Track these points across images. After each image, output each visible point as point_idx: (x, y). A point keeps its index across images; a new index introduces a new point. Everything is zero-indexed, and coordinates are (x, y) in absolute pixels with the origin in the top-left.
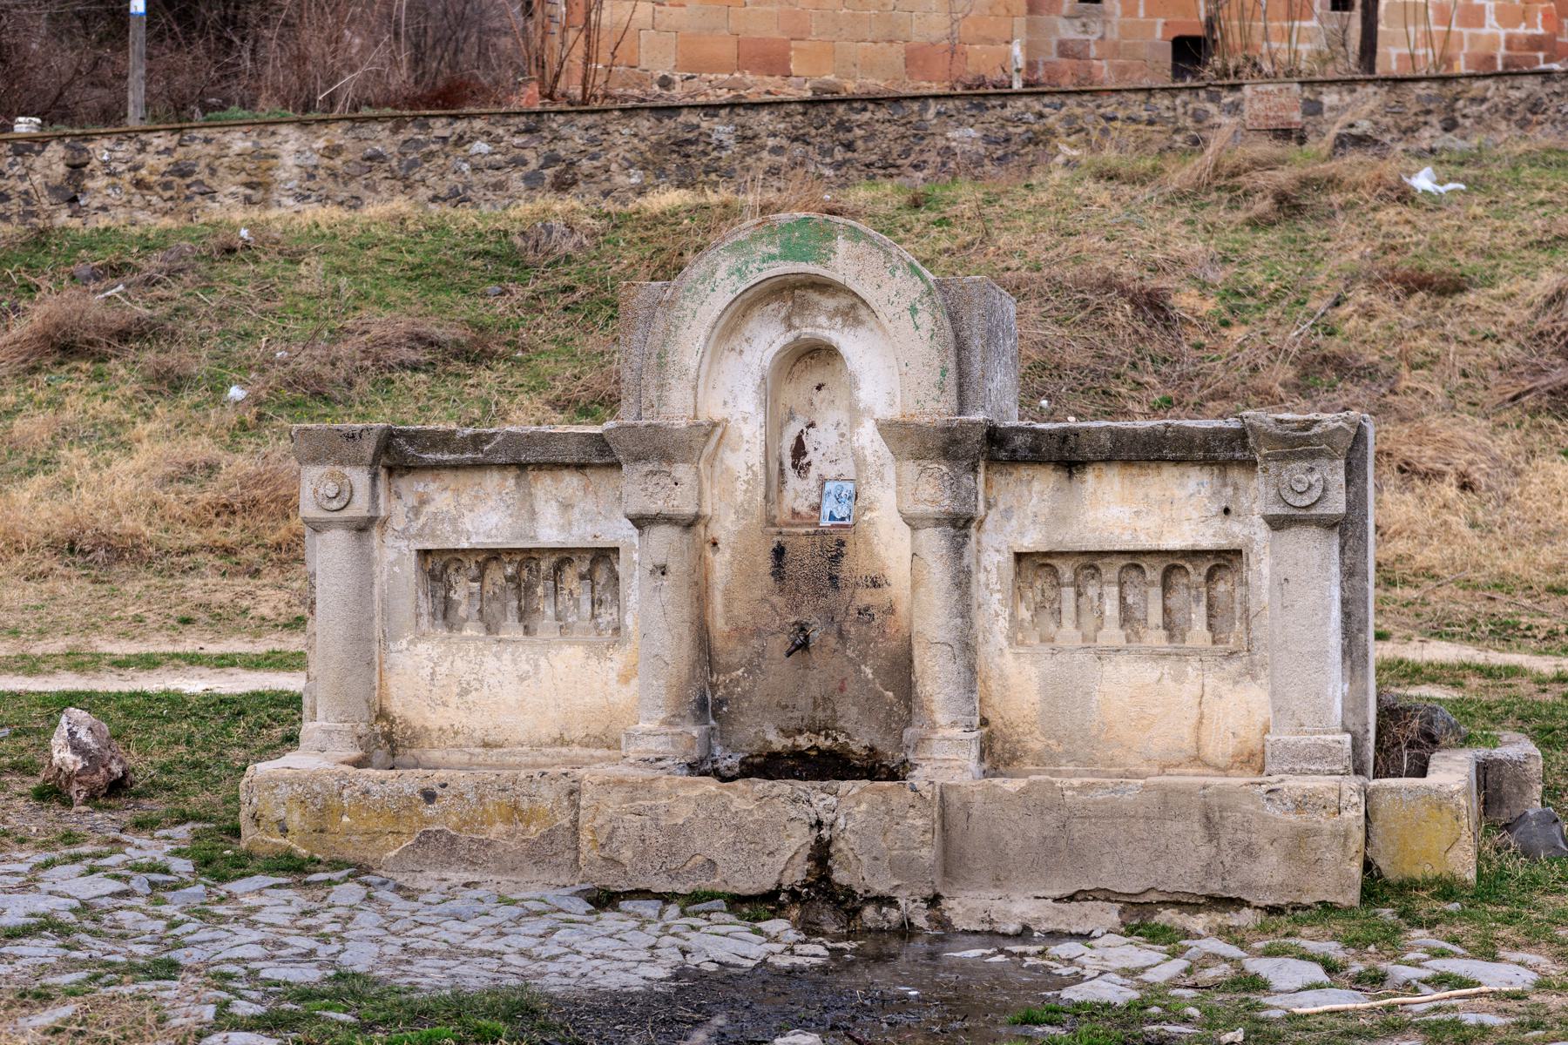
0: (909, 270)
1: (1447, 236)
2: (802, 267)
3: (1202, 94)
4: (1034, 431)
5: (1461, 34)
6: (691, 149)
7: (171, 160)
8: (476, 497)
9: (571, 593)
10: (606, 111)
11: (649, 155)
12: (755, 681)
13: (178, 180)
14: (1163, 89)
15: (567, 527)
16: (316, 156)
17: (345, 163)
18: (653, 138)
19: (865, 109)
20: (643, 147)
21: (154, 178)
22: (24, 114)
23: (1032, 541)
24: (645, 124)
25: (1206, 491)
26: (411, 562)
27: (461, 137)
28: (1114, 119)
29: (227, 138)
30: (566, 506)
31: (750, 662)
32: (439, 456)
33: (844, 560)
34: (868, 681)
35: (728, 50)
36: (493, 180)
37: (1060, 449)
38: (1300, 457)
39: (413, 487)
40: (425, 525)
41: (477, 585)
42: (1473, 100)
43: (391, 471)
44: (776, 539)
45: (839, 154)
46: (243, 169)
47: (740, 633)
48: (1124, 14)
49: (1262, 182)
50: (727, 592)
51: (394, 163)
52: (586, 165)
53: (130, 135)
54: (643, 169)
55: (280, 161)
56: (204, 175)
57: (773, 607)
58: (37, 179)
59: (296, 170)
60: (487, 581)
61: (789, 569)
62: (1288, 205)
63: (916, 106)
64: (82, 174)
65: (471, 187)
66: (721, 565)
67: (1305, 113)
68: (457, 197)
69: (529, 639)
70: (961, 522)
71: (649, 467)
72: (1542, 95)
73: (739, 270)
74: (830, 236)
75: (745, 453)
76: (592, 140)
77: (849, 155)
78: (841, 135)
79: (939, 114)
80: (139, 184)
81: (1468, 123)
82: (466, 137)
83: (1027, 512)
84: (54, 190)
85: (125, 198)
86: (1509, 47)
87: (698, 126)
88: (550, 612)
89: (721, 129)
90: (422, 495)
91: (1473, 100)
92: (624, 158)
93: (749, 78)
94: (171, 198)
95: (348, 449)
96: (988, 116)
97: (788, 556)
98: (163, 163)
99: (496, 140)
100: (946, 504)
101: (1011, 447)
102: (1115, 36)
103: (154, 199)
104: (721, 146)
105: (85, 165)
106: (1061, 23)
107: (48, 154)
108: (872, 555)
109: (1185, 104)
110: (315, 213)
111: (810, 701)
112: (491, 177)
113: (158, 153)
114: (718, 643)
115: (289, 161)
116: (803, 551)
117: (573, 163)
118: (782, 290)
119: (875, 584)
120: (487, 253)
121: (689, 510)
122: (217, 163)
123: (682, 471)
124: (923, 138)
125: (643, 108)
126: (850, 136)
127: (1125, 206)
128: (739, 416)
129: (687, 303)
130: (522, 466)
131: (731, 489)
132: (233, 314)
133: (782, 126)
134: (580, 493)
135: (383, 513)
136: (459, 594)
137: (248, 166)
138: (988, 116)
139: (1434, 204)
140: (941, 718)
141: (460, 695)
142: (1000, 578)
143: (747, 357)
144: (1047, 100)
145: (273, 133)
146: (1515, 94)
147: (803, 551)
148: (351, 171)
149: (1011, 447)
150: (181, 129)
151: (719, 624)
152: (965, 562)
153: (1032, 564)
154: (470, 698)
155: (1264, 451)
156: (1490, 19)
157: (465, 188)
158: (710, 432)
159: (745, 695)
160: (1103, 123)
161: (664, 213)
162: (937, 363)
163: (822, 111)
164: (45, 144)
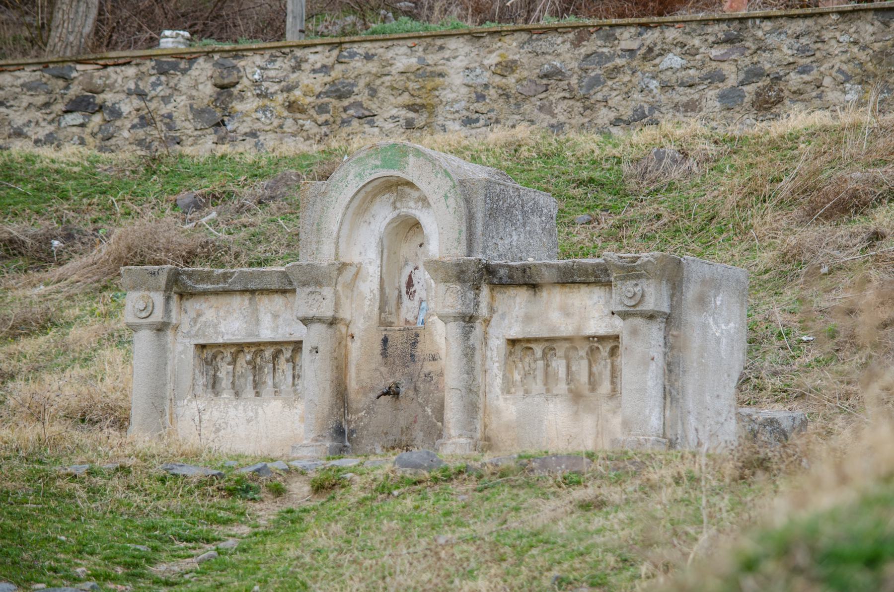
0: (444, 174)
2: (391, 172)
4: (508, 266)
7: (327, 79)
8: (228, 312)
9: (283, 372)
11: (870, 66)
12: (370, 418)
13: (335, 102)
15: (275, 328)
16: (487, 74)
17: (518, 81)
18: (877, 46)
20: (863, 56)
21: (308, 100)
22: (171, 28)
23: (515, 332)
25: (602, 301)
26: (191, 351)
27: (650, 50)
29: (390, 54)
30: (276, 316)
31: (369, 407)
32: (205, 286)
33: (418, 345)
34: (428, 417)
36: (685, 99)
37: (524, 277)
38: (632, 278)
39: (193, 305)
40: (199, 329)
41: (231, 367)
43: (181, 296)
44: (384, 333)
46: (406, 89)
47: (365, 391)
50: (358, 366)
51: (574, 81)
52: (794, 80)
53: (285, 51)
55: (447, 80)
56: (363, 97)
57: (381, 373)
58: (181, 100)
59: (464, 90)
60: (238, 364)
61: (390, 351)
64: (230, 95)
65: (658, 108)
66: (355, 349)
68: (640, 118)
69: (259, 398)
70: (467, 319)
71: (310, 289)
73: (360, 174)
75: (369, 286)
80: (291, 106)
82: (656, 50)
83: (513, 314)
84: (199, 113)
85: (276, 123)
88: (270, 382)
90: (199, 310)
92: (840, 71)
94: (326, 123)
95: (152, 281)
97: (390, 343)
98: (317, 83)
100: (459, 308)
101: (498, 276)
103: (308, 124)
105: (234, 85)
107: (194, 73)
108: (433, 342)
111: (400, 429)
112: (682, 95)
113: (314, 71)
114: (352, 396)
115: (456, 79)
116: (398, 340)
118: (392, 186)
119: (434, 359)
120: (591, 180)
121: (327, 312)
122: (378, 82)
123: (327, 291)
128: (367, 261)
129: (333, 194)
130: (253, 292)
131: (361, 311)
134: (283, 309)
135: (174, 321)
136: (221, 374)
137: (411, 85)
141: (215, 433)
142: (498, 354)
143: (372, 227)
145: (441, 48)
147: (398, 340)
148: (524, 91)
149: (498, 276)
150: (341, 43)
151: (353, 385)
152: (471, 342)
153: (516, 344)
154: (220, 434)
155: (615, 275)
157: (652, 109)
159: (365, 427)
162: (457, 227)
164: (192, 61)
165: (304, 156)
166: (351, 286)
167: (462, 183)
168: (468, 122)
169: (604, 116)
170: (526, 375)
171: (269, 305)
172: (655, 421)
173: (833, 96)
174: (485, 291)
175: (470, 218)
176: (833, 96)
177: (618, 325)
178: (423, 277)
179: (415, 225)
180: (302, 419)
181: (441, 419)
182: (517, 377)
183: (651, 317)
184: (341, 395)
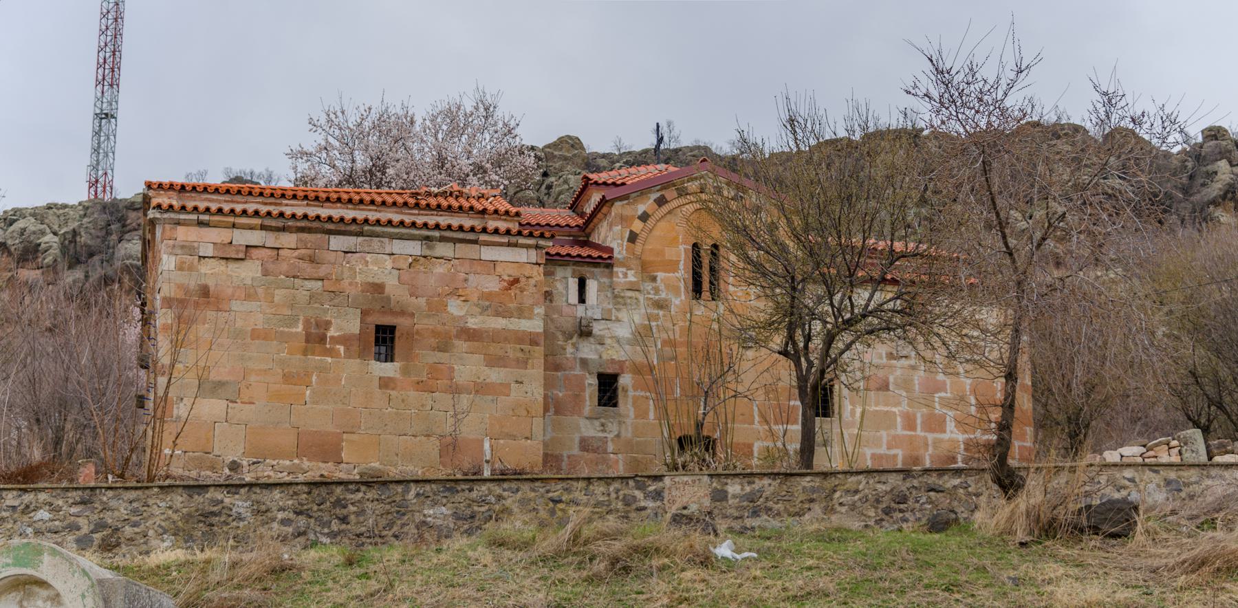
1: (727, 592)
2: (29, 571)
3: (631, 483)
5: (926, 438)
6: (215, 520)
10: (147, 488)
11: (180, 524)
14: (600, 479)
18: (185, 511)
19: (358, 490)
20: (175, 517)
24: (178, 499)
27: (27, 507)
28: (560, 501)
35: (289, 440)
45: (335, 526)
48: (636, 418)
49: (603, 549)
54: (175, 535)
62: (620, 567)
63: (400, 489)
67: (714, 499)
72: (904, 488)
76: (135, 512)
77: (344, 526)
78: (338, 511)
79: (418, 495)
81: (843, 509)
82: (32, 507)
87: (222, 502)
89: (240, 504)
92: (160, 526)
93: (306, 464)
96: (458, 498)
102: (629, 435)
104: (240, 518)
106: (583, 423)
109: (617, 491)
117: (117, 529)
124: (404, 514)
125: (178, 486)
126: (345, 512)
127: (501, 565)
133: (290, 502)
138: (458, 497)
139: (730, 565)
144: (506, 485)
146: (881, 487)
156: (950, 425)
160: (551, 505)
161: (158, 567)
163: (323, 491)
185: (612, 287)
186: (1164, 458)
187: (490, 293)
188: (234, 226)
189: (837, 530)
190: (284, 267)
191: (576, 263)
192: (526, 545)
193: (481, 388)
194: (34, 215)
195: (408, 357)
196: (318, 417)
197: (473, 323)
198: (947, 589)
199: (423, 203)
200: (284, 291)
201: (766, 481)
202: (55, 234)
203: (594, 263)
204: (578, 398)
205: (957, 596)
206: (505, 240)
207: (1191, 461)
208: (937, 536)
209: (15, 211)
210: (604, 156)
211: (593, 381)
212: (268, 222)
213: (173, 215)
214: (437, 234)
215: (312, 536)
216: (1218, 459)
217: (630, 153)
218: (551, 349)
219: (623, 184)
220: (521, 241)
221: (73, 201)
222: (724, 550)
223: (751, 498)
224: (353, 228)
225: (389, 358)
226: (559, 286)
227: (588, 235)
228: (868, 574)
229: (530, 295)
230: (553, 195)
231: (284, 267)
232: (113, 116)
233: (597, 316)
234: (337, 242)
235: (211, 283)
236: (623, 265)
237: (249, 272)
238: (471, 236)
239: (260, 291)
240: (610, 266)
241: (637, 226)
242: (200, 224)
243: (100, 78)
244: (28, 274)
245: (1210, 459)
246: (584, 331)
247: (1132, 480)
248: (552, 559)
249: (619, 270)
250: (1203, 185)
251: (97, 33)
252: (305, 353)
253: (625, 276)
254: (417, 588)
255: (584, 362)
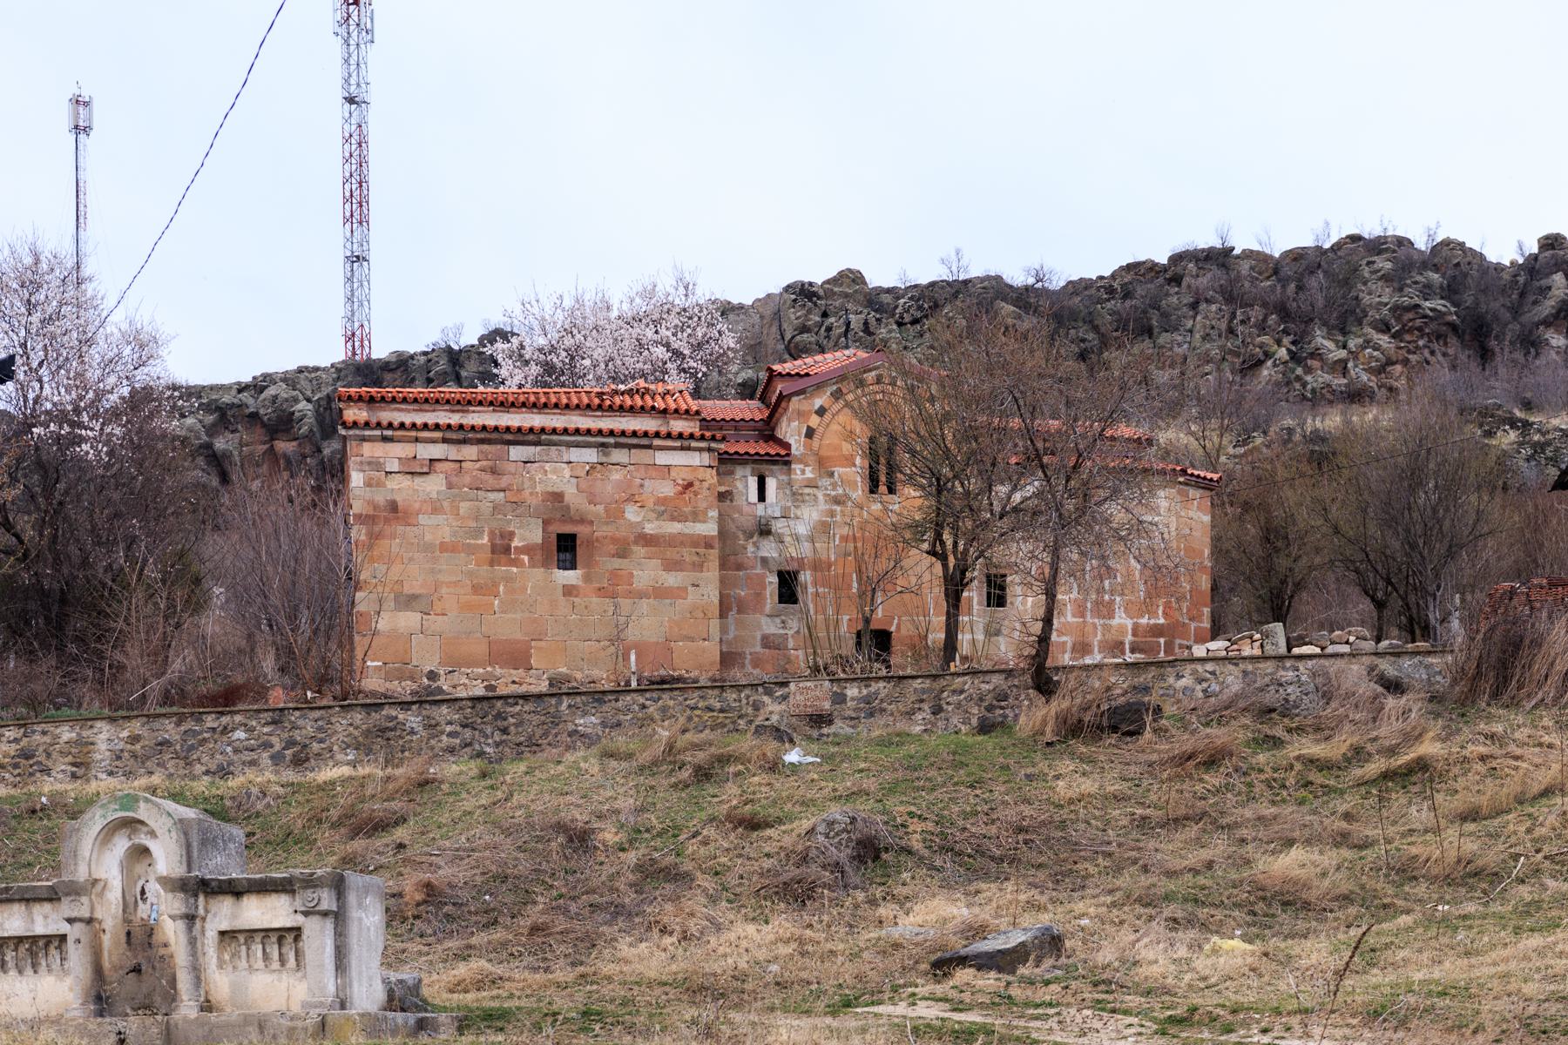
3: (760, 689)
13: (24, 761)
15: (46, 926)
20: (356, 733)
23: (224, 926)
24: (358, 717)
30: (46, 917)
35: (481, 649)
42: (954, 692)
47: (115, 968)
52: (316, 746)
56: (42, 758)
66: (107, 940)
67: (834, 703)
74: (137, 801)
75: (114, 895)
76: (320, 729)
79: (570, 706)
83: (223, 914)
86: (1134, 635)
89: (413, 719)
91: (954, 692)
93: (498, 671)
96: (605, 708)
99: (252, 730)
104: (412, 732)
106: (764, 620)
110: (112, 782)
112: (247, 756)
115: (103, 747)
116: (138, 934)
121: (87, 915)
123: (84, 899)
130: (28, 900)
131: (109, 910)
132: (23, 852)
140: (185, 997)
144: (648, 695)
146: (985, 687)
147: (138, 934)
151: (106, 965)
153: (226, 936)
158: (94, 885)
159: (118, 994)
163: (485, 705)
165: (13, 797)
166: (101, 895)
167: (181, 821)
168: (111, 774)
169: (199, 769)
170: (233, 955)
171: (40, 910)
172: (331, 988)
173: (340, 757)
174: (201, 898)
175: (188, 846)
176: (340, 757)
177: (299, 920)
178: (153, 888)
179: (145, 851)
180: (71, 989)
181: (175, 988)
182: (227, 957)
183: (325, 914)
184: (98, 971)
185: (789, 483)
186: (1247, 652)
187: (665, 498)
188: (417, 440)
189: (898, 735)
190: (467, 479)
191: (755, 462)
192: (629, 756)
193: (660, 593)
194: (284, 380)
195: (589, 565)
196: (507, 626)
197: (650, 528)
198: (972, 786)
199: (608, 403)
200: (468, 504)
201: (881, 684)
202: (309, 400)
203: (773, 460)
204: (759, 596)
205: (978, 792)
206: (678, 444)
207: (1273, 654)
208: (980, 738)
209: (265, 376)
210: (889, 291)
211: (775, 579)
212: (449, 435)
213: (357, 432)
214: (611, 440)
215: (477, 747)
216: (1296, 651)
217: (916, 286)
218: (728, 551)
219: (807, 375)
220: (694, 444)
221: (325, 363)
222: (793, 757)
223: (867, 700)
224: (531, 437)
225: (573, 567)
226: (739, 485)
227: (773, 429)
228: (909, 775)
229: (705, 498)
230: (833, 338)
231: (467, 479)
232: (365, 259)
233: (778, 514)
234: (517, 452)
235: (398, 499)
236: (801, 462)
237: (434, 485)
238: (645, 441)
239: (445, 504)
240: (788, 463)
241: (814, 421)
242: (385, 439)
243: (348, 214)
244: (284, 446)
245: (1289, 650)
246: (764, 531)
247: (1213, 673)
248: (651, 768)
249: (796, 467)
250: (1535, 303)
251: (340, 161)
252: (492, 564)
253: (803, 472)
254: (532, 797)
255: (764, 561)
